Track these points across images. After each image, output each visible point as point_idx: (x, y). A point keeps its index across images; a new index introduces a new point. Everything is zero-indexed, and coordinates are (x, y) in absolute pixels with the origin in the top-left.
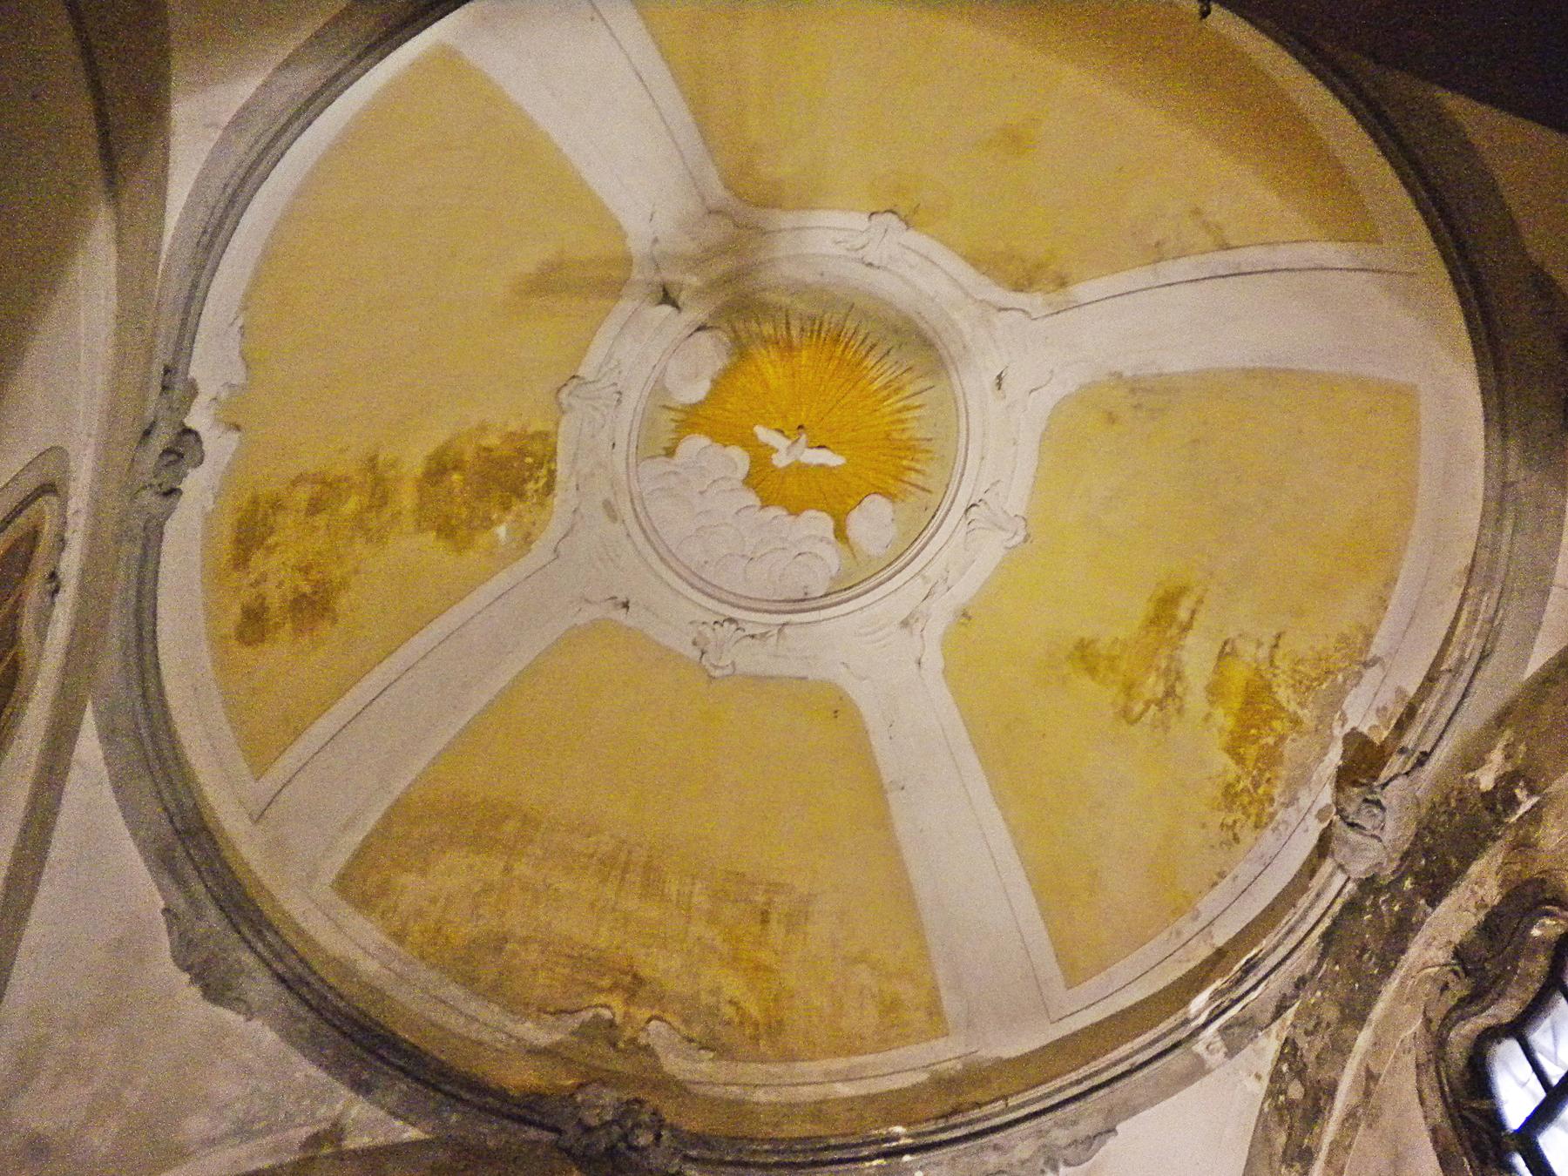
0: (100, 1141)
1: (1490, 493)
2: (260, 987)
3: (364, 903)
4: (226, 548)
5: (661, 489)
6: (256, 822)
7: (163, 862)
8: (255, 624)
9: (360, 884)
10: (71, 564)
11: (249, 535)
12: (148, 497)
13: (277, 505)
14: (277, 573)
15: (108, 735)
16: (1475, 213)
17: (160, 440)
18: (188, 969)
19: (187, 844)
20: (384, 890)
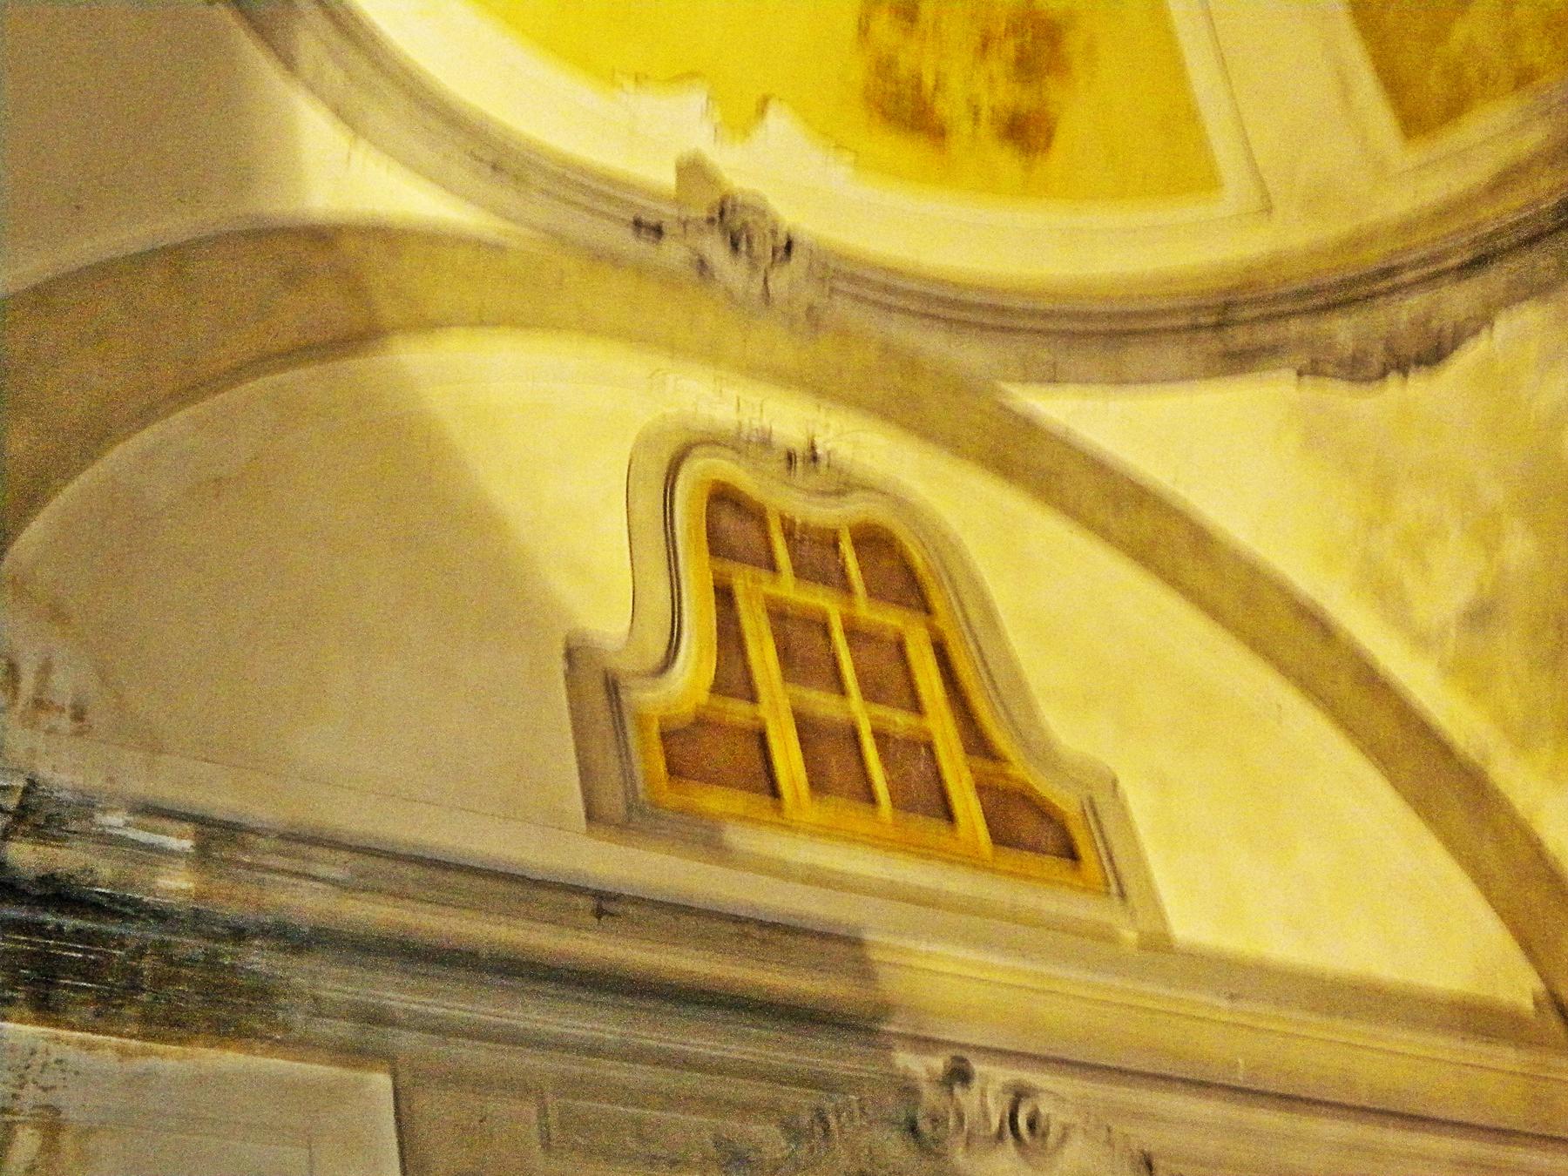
0: (1520, 548)
1: (16, 1016)
2: (1459, 299)
3: (1455, 108)
4: (908, 151)
5: (172, 964)
6: (1268, 210)
7: (1239, 361)
8: (1025, 132)
9: (1421, 112)
10: (790, 418)
11: (908, 112)
12: (781, 281)
13: (884, 67)
14: (969, 85)
15: (1053, 377)
16: (70, 394)
17: (715, 249)
18: (1383, 375)
19: (1225, 327)
20: (1455, 73)
